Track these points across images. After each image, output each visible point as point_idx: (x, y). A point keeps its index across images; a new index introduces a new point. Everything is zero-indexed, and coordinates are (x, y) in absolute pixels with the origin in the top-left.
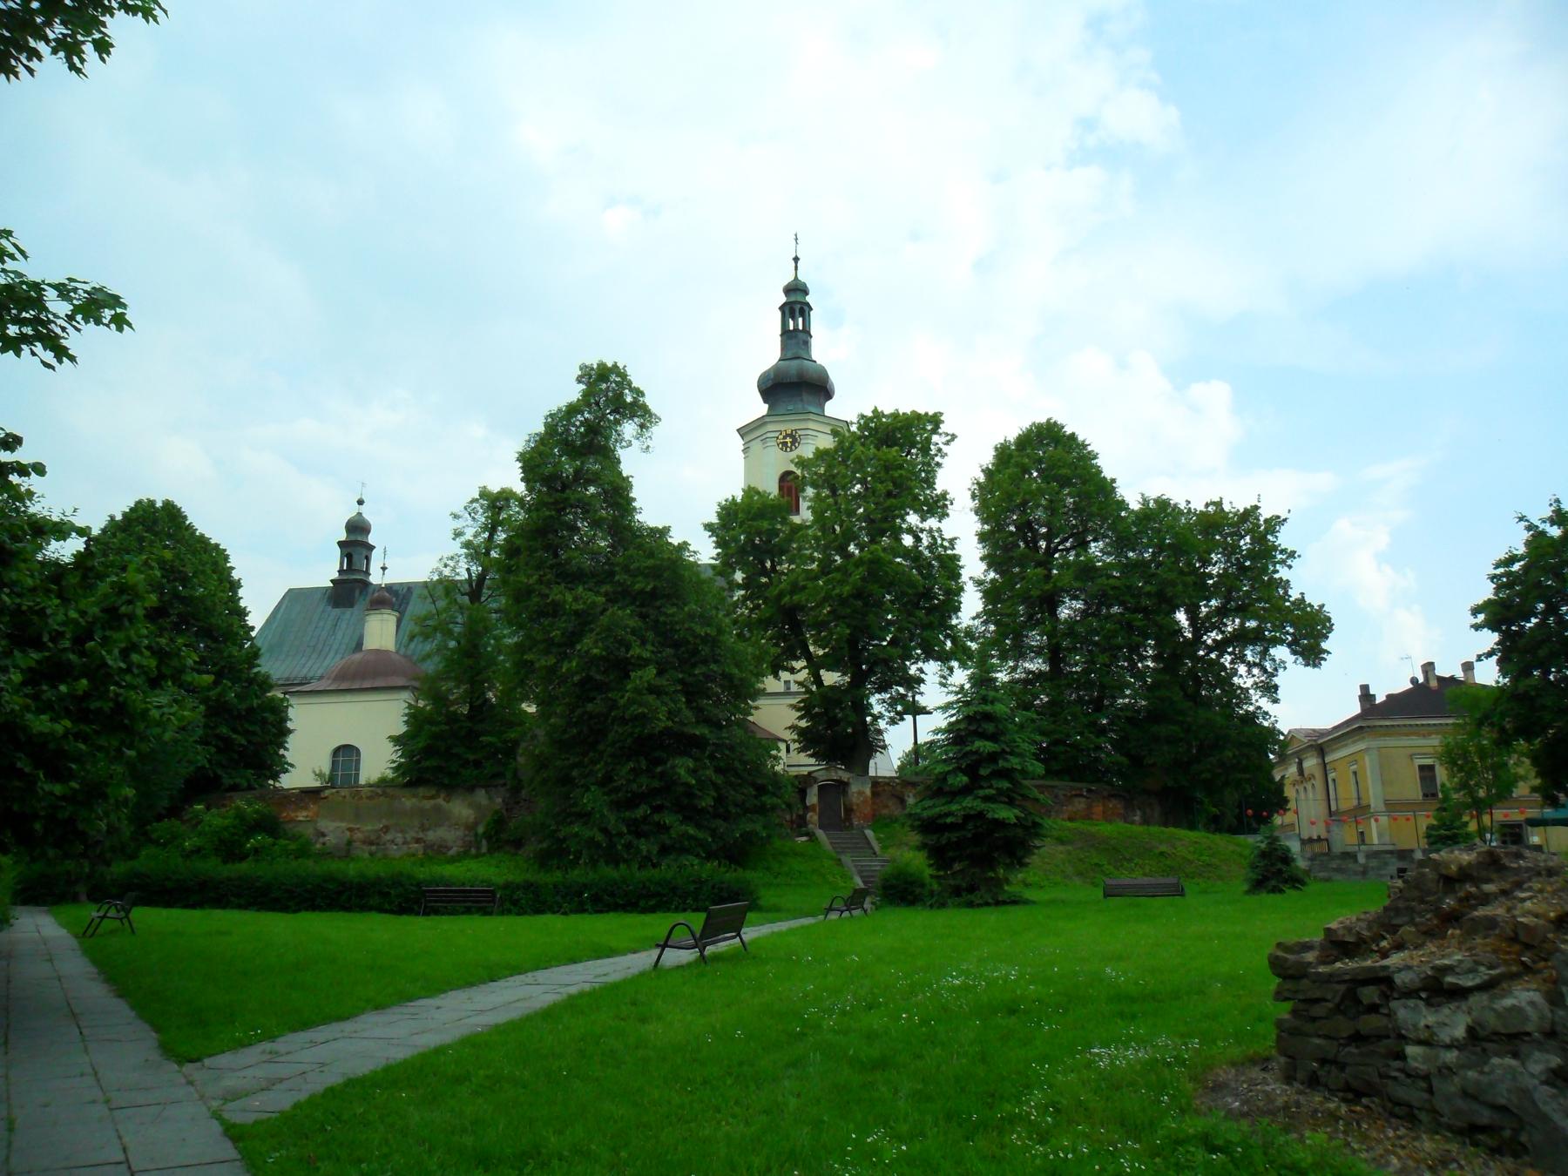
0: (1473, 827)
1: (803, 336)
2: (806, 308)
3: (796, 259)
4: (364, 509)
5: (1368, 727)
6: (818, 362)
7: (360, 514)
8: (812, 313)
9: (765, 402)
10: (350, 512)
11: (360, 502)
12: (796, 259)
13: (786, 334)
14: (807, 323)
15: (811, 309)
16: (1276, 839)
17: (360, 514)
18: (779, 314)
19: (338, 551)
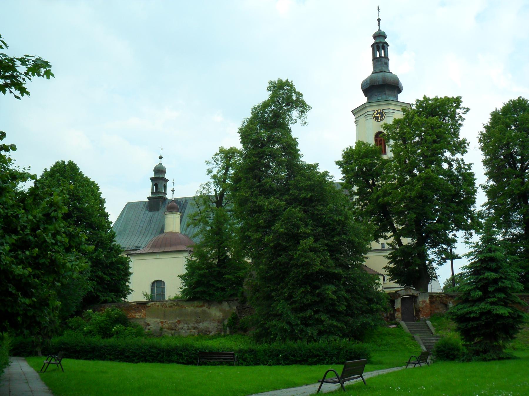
2: (385, 45)
3: (379, 20)
7: (160, 164)
8: (389, 47)
9: (366, 96)
11: (161, 158)
12: (379, 20)
13: (375, 59)
15: (388, 45)
17: (160, 164)
18: (371, 49)
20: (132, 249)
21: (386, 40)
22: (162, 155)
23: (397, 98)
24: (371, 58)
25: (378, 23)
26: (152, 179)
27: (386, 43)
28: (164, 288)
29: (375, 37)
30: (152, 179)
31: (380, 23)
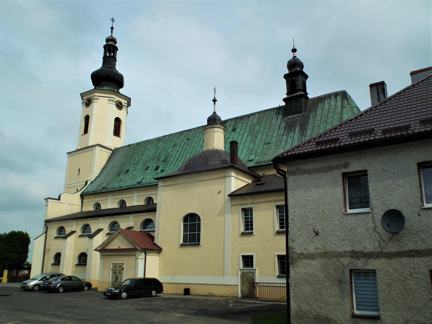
0: (417, 270)
1: (112, 59)
2: (116, 49)
3: (112, 28)
4: (296, 54)
5: (47, 264)
6: (119, 72)
7: (294, 57)
8: (117, 51)
9: (94, 85)
10: (290, 56)
11: (294, 50)
12: (112, 28)
13: (105, 58)
14: (105, 54)
15: (117, 50)
16: (341, 294)
17: (294, 57)
18: (103, 50)
19: (284, 81)
20: (131, 187)
21: (116, 45)
22: (295, 47)
23: (119, 89)
24: (102, 56)
25: (111, 30)
26: (286, 76)
27: (116, 48)
28: (199, 225)
29: (107, 40)
30: (286, 76)
31: (113, 30)
